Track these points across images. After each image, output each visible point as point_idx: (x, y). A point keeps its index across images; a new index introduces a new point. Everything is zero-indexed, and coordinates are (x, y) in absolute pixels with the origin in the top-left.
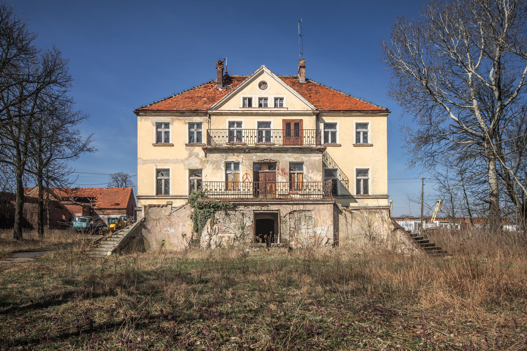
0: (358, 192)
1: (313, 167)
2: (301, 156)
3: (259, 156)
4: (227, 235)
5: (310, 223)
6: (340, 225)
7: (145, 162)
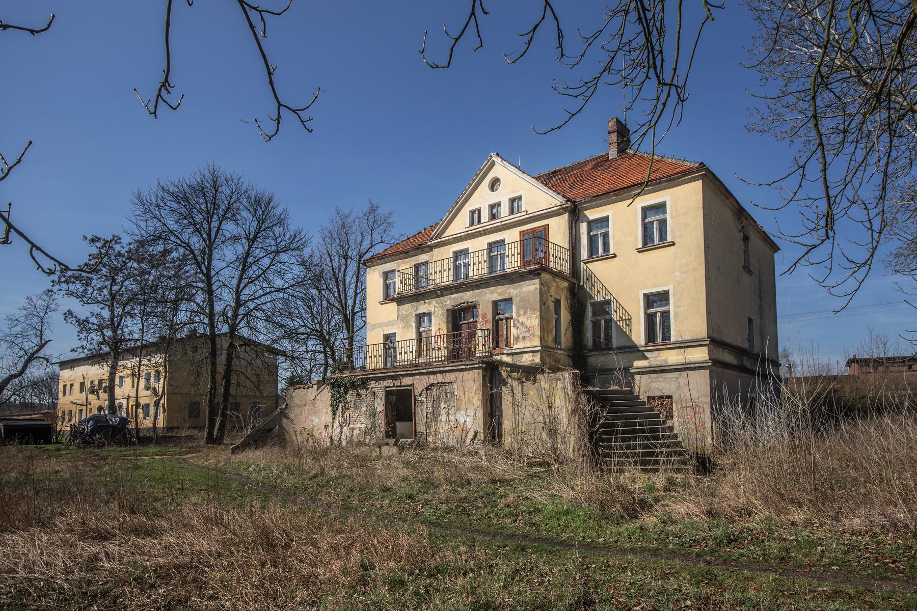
0: (651, 336)
1: (526, 307)
2: (508, 289)
3: (454, 299)
4: (358, 426)
5: (452, 404)
6: (504, 406)
7: (374, 327)
